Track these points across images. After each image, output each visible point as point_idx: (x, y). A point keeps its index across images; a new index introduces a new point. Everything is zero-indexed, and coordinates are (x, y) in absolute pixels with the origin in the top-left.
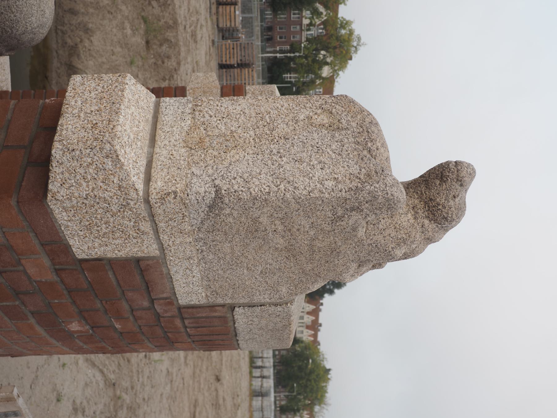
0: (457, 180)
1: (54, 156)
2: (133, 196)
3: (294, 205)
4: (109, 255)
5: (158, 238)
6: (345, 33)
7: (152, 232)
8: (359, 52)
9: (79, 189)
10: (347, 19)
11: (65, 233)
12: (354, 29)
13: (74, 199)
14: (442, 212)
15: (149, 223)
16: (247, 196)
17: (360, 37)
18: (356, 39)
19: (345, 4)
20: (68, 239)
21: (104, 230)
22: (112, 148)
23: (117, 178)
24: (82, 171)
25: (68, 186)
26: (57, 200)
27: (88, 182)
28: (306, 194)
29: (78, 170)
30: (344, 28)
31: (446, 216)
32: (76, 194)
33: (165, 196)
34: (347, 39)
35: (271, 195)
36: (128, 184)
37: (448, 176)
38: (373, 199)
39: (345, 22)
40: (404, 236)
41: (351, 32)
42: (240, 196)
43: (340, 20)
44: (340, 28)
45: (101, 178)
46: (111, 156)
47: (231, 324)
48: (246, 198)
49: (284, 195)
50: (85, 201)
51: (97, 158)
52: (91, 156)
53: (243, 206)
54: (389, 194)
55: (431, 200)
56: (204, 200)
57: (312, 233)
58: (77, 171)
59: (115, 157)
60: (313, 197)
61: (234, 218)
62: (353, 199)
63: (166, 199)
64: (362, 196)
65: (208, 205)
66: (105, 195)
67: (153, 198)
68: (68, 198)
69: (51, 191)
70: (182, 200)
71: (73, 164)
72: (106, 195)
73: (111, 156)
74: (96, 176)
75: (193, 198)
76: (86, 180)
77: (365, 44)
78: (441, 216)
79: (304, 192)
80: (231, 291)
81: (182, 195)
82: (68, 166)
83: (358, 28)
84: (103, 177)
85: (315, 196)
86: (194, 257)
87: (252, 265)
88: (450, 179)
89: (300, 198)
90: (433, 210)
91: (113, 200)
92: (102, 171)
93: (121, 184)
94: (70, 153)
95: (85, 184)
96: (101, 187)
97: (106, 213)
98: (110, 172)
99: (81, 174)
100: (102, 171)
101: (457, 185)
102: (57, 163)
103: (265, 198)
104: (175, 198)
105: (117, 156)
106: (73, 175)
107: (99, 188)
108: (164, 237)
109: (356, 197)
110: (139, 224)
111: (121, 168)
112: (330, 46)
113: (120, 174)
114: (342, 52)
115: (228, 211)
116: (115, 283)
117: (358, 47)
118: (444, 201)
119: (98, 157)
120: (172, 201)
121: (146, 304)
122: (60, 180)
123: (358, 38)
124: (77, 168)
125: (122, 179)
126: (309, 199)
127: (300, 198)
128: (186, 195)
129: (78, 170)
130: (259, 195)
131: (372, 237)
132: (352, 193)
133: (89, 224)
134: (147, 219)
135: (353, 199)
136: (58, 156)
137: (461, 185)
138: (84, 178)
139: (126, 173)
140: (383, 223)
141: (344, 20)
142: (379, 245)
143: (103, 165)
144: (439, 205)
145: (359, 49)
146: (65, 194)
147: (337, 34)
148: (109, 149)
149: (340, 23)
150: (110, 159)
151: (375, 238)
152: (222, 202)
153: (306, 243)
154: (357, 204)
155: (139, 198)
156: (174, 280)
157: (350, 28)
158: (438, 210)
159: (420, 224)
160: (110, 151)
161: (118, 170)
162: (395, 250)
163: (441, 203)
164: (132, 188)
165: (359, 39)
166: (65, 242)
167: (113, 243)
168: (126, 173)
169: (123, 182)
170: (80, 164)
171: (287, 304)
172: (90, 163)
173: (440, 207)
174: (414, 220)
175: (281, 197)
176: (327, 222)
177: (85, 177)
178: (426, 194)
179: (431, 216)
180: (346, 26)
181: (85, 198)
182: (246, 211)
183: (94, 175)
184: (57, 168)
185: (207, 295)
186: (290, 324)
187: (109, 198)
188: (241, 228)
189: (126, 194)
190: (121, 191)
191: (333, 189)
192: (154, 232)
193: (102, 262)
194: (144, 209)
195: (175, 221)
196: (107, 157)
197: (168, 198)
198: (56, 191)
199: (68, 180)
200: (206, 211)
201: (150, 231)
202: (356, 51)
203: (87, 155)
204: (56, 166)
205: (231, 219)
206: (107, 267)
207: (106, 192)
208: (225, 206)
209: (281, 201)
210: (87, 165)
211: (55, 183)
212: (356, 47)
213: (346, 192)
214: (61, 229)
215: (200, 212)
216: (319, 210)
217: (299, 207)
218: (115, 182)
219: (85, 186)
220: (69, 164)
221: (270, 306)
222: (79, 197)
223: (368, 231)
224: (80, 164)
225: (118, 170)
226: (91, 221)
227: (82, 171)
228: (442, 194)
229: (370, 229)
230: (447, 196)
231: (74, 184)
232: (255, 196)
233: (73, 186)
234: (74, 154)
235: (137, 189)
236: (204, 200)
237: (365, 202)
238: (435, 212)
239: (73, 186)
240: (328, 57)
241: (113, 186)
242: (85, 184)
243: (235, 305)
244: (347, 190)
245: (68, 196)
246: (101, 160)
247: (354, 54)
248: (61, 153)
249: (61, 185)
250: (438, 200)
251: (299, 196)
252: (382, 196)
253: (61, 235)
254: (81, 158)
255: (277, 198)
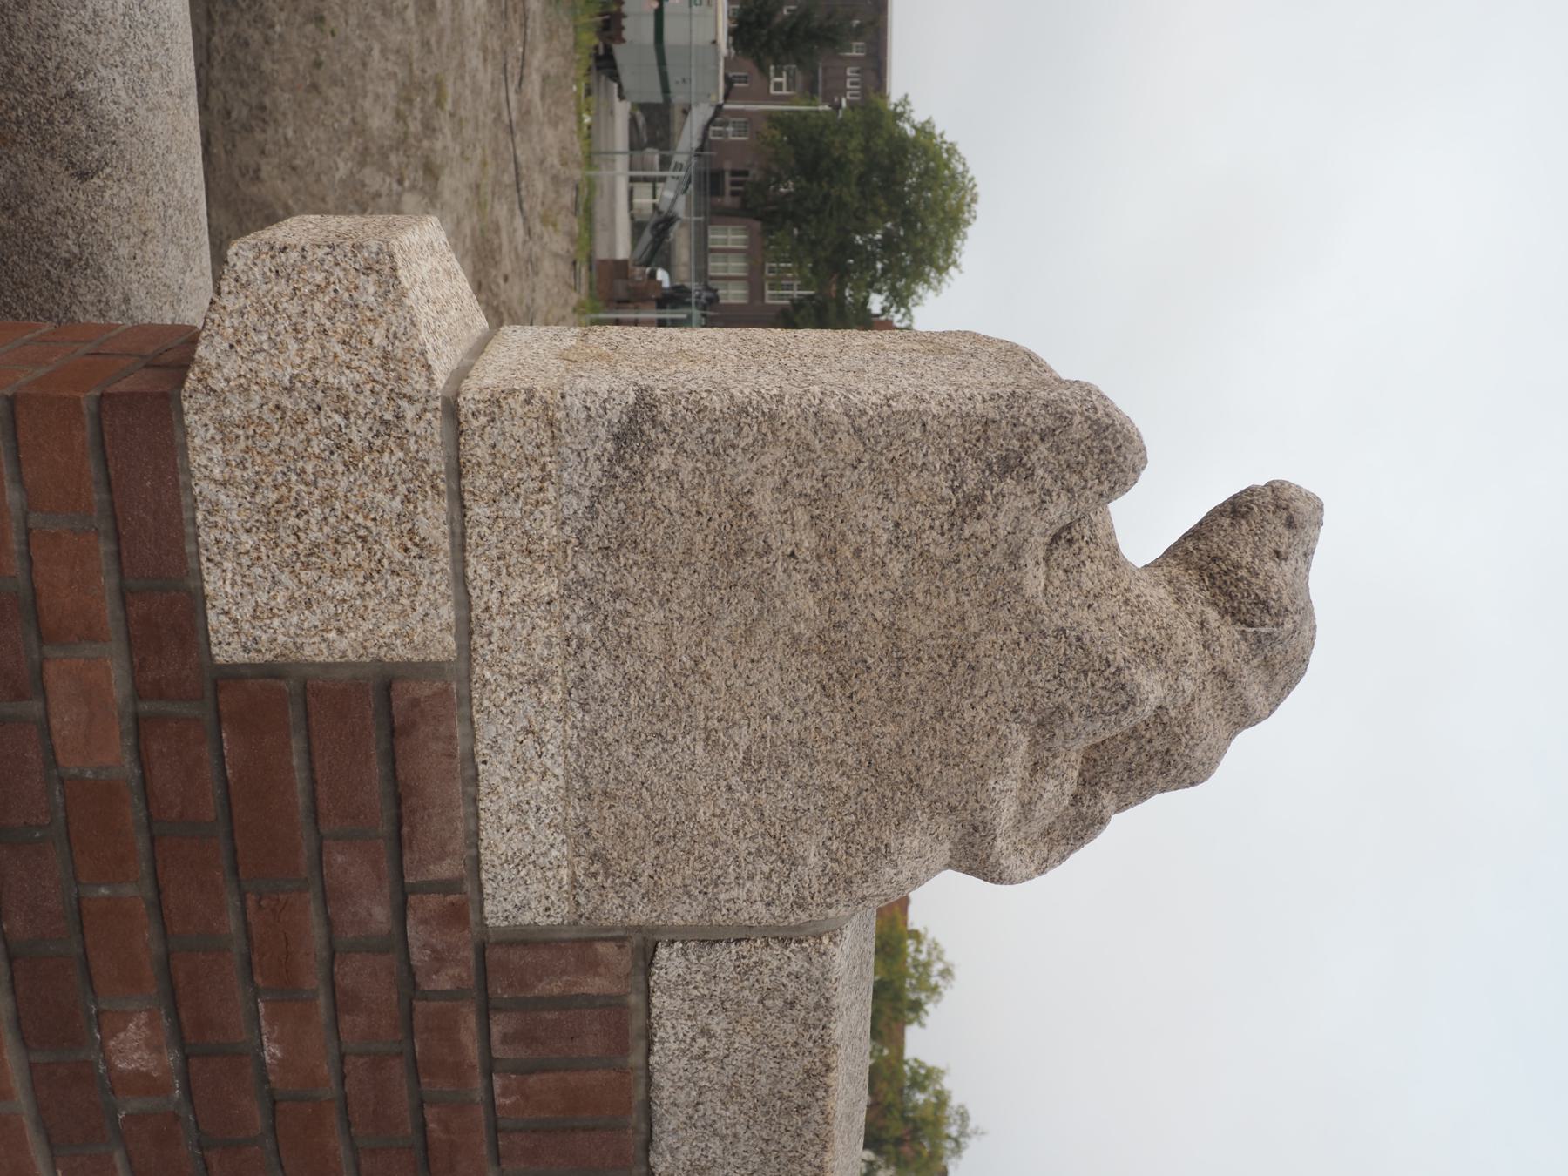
0: (1278, 507)
1: (231, 264)
2: (418, 386)
3: (848, 445)
4: (315, 651)
5: (460, 563)
6: (925, 1101)
7: (447, 546)
8: (965, 1154)
9: (275, 360)
10: (930, 1063)
11: (203, 538)
12: (950, 1092)
13: (256, 388)
14: (1249, 584)
15: (445, 504)
16: (722, 401)
17: (966, 1112)
18: (958, 1117)
19: (922, 1025)
20: (205, 565)
21: (315, 535)
22: (384, 246)
23: (383, 332)
24: (294, 308)
25: (248, 349)
26: (210, 391)
27: (303, 341)
28: (879, 402)
29: (286, 305)
30: (923, 1089)
31: (1262, 595)
32: (265, 375)
33: (503, 395)
34: (931, 1118)
35: (786, 401)
36: (408, 349)
37: (1251, 501)
38: (1058, 423)
39: (923, 1072)
40: (1154, 633)
41: (942, 1100)
42: (702, 402)
43: (911, 1068)
44: (910, 1087)
45: (340, 331)
46: (377, 267)
47: (636, 1059)
48: (718, 406)
49: (821, 401)
50: (286, 402)
51: (341, 274)
52: (326, 267)
53: (710, 436)
54: (1100, 413)
55: (1214, 559)
56: (605, 409)
57: (895, 568)
58: (280, 307)
59: (387, 271)
60: (898, 412)
61: (682, 494)
62: (1004, 422)
63: (503, 404)
64: (1028, 414)
65: (615, 430)
66: (343, 379)
67: (469, 397)
68: (241, 385)
69: (199, 363)
70: (546, 409)
71: (276, 289)
72: (346, 380)
73: (377, 267)
74: (328, 324)
75: (577, 403)
76: (300, 336)
77: (983, 1133)
78: (1249, 595)
79: (874, 399)
80: (652, 852)
81: (547, 396)
82: (260, 292)
83: (959, 1089)
84: (346, 326)
85: (902, 408)
86: (554, 673)
87: (720, 720)
88: (1258, 506)
89: (864, 413)
90: (1225, 582)
91: (361, 398)
92: (348, 310)
93: (390, 348)
94: (272, 257)
95: (296, 346)
96: (335, 356)
97: (332, 453)
98: (368, 314)
99: (289, 317)
100: (348, 310)
101: (1277, 521)
102: (233, 283)
103: (770, 409)
104: (527, 402)
105: (394, 269)
106: (267, 318)
107: (330, 359)
108: (478, 568)
109: (1012, 417)
110: (416, 507)
111: (399, 301)
112: (884, 1135)
113: (393, 318)
114: (919, 1154)
115: (663, 461)
116: (302, 800)
117: (962, 1140)
118: (1250, 559)
119: (345, 270)
120: (520, 411)
121: (380, 915)
122: (231, 330)
123: (962, 1115)
124: (284, 300)
125: (395, 334)
126: (889, 417)
127: (864, 413)
128: (559, 397)
129: (286, 305)
130: (754, 402)
131: (1064, 610)
132: (1003, 404)
133: (278, 502)
134: (442, 486)
135: (1004, 422)
136: (240, 265)
137: (1290, 523)
138: (295, 330)
139: (408, 316)
140: (1091, 573)
141: (921, 1065)
142: (1086, 639)
143: (353, 293)
144: (1237, 567)
145: (967, 1146)
146: (235, 375)
147: (902, 1103)
148: (375, 249)
149: (909, 1074)
150: (374, 277)
151: (1075, 615)
152: (653, 420)
153: (879, 615)
154: (1016, 444)
155: (433, 391)
156: (483, 789)
157: (938, 1087)
158: (1238, 579)
159: (1194, 617)
160: (378, 254)
161: (389, 309)
162: (1133, 670)
163: (1244, 563)
164: (417, 360)
165: (964, 1116)
166: (192, 584)
167: (329, 592)
168: (408, 316)
169: (397, 343)
170: (295, 289)
171: (820, 938)
172: (318, 286)
173: (1243, 573)
174: (1176, 606)
175: (812, 409)
176: (937, 523)
177: (299, 327)
178: (1199, 550)
179: (1222, 599)
180: (927, 1083)
181: (286, 389)
182: (715, 460)
183: (324, 321)
184: (232, 297)
185: (574, 882)
186: (828, 1069)
187: (351, 389)
188: (698, 538)
189: (399, 378)
190: (387, 371)
191: (949, 395)
192: (453, 545)
193: (283, 683)
194: (438, 439)
195: (518, 496)
196: (368, 270)
197: (510, 400)
198: (213, 364)
199: (252, 333)
200: (606, 455)
201: (441, 540)
202: (958, 1148)
203: (316, 263)
204: (229, 293)
205: (673, 494)
206: (294, 714)
207: (347, 372)
208: (661, 436)
209: (812, 421)
210: (311, 291)
211: (218, 339)
212: (956, 1141)
213: (984, 401)
214: (194, 519)
215: (592, 460)
216: (914, 466)
217: (861, 448)
218: (376, 342)
219: (293, 352)
220: (265, 287)
221: (768, 945)
222: (272, 384)
223: (1050, 589)
224: (295, 289)
225: (389, 309)
226: (284, 490)
227: (294, 308)
228: (1242, 544)
229: (1057, 583)
230: (1257, 547)
231: (266, 347)
232: (743, 403)
233: (262, 350)
234: (283, 259)
235: (430, 366)
236: (605, 409)
237: (1037, 437)
238: (1233, 588)
239: (262, 350)
240: (880, 1167)
241: (367, 353)
242: (293, 346)
243: (657, 937)
244: (987, 398)
245: (243, 380)
246: (351, 278)
247: (954, 1160)
248: (251, 255)
249: (231, 346)
250: (1233, 556)
251: (861, 406)
252: (1082, 414)
253: (190, 548)
254: (299, 273)
255: (803, 411)
